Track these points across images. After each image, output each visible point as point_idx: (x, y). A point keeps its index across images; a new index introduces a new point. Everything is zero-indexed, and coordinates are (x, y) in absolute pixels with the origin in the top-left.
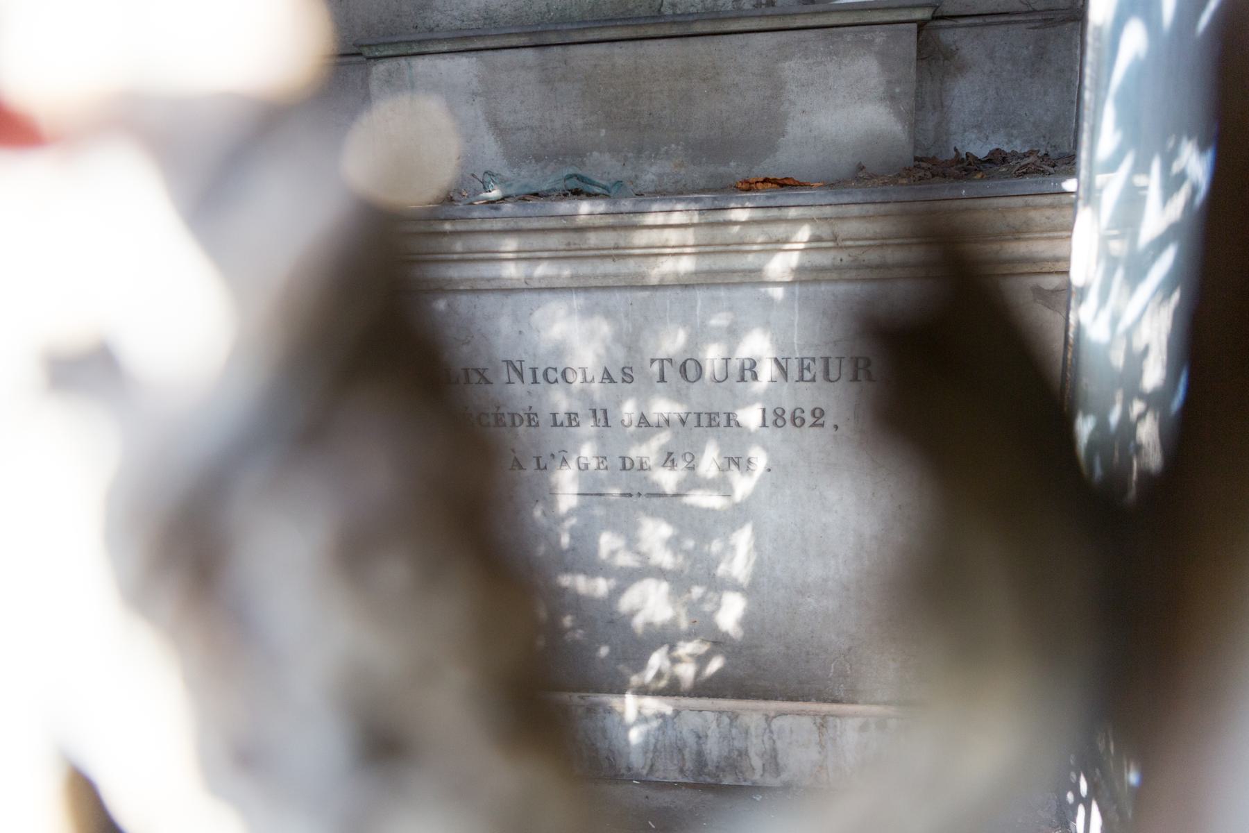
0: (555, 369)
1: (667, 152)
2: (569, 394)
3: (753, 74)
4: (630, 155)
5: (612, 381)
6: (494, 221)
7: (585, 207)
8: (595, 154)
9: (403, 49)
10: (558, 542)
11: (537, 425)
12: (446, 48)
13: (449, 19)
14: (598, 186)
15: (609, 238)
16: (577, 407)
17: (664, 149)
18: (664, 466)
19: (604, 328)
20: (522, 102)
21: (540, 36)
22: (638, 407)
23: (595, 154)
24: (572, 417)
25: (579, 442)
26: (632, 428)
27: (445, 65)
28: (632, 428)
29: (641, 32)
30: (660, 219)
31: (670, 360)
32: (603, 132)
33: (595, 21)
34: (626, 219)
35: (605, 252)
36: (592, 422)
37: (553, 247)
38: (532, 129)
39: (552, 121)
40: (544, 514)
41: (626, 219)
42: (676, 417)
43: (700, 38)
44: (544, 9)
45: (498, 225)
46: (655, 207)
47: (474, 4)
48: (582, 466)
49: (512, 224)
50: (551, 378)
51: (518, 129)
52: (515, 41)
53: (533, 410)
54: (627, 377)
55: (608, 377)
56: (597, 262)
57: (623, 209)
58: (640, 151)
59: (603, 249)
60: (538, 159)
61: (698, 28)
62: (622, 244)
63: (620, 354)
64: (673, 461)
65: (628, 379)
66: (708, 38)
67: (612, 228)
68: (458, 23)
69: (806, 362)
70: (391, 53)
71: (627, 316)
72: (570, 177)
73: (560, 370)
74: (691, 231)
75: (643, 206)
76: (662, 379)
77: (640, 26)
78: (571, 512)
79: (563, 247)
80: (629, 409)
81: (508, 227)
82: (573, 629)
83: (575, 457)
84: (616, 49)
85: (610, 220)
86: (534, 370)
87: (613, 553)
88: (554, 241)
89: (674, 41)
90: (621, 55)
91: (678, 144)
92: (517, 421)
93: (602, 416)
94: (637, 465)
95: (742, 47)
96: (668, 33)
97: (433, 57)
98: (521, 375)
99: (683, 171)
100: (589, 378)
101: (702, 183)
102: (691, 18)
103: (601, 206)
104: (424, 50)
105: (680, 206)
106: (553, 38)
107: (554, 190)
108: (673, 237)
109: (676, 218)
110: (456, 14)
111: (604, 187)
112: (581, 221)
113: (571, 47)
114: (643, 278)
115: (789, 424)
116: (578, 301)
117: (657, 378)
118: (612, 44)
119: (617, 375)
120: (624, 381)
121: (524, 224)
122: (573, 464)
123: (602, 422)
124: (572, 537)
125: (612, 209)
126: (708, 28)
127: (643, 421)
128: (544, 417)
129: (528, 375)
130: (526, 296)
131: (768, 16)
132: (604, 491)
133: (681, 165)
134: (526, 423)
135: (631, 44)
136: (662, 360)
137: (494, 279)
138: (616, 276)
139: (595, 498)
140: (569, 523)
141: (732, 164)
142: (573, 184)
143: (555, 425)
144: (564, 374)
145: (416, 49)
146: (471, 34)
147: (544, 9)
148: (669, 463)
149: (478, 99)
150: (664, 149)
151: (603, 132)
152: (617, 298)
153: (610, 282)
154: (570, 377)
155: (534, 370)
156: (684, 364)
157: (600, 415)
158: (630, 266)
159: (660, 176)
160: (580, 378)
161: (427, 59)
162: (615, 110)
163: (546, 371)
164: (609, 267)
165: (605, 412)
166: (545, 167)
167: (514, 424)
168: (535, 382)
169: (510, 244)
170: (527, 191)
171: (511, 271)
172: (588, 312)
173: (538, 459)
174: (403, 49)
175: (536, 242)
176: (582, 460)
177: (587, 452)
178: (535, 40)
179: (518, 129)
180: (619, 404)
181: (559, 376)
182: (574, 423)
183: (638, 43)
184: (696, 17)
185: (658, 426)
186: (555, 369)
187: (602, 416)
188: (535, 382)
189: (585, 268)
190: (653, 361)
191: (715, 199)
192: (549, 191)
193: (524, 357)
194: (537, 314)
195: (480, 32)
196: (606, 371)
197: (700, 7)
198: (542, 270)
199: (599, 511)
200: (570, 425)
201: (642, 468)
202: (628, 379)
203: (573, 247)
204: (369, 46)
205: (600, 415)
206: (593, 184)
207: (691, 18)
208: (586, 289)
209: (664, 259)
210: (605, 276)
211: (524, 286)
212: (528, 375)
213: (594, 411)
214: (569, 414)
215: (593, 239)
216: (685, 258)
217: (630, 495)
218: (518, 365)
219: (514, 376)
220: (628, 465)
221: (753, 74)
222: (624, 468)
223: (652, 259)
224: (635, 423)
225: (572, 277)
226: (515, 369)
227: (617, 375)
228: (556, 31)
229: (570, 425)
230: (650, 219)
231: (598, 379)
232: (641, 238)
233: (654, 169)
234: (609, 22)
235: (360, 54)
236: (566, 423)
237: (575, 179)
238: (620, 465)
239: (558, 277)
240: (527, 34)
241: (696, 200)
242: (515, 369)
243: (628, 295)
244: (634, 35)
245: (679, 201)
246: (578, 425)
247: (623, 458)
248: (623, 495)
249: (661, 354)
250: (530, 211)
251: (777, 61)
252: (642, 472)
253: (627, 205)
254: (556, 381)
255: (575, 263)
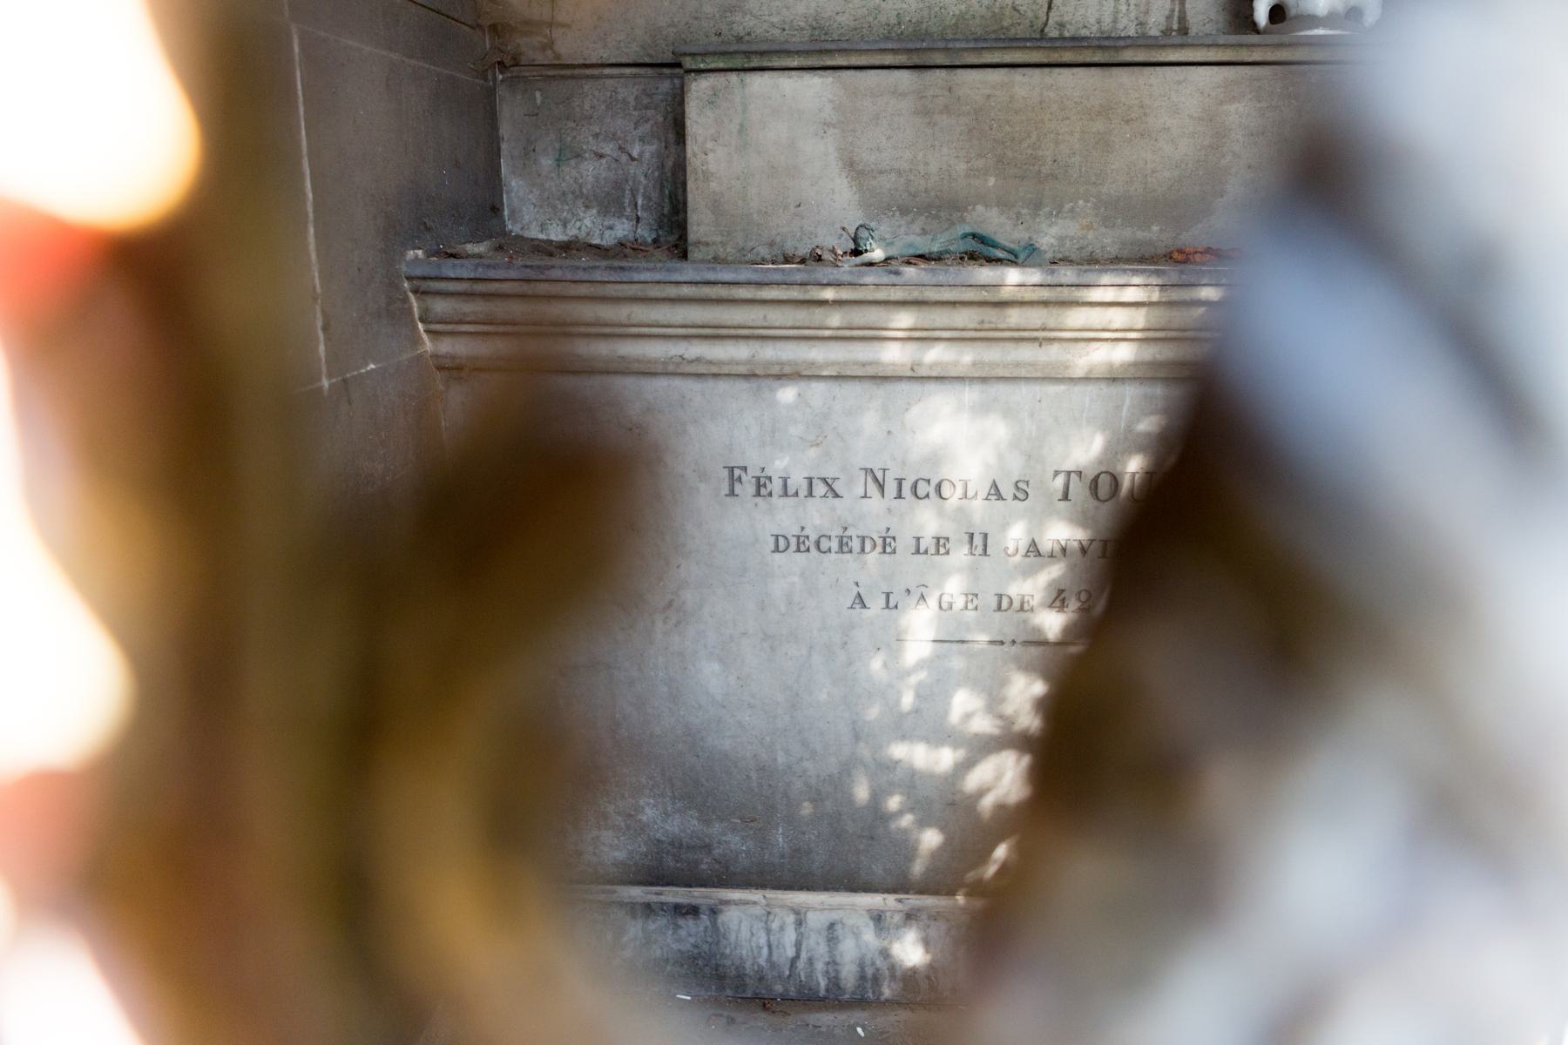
0: (929, 481)
1: (1072, 210)
2: (941, 513)
3: (1191, 117)
4: (1024, 211)
5: (1000, 497)
6: (893, 289)
7: (1013, 276)
8: (979, 208)
9: (739, 62)
10: (898, 702)
11: (894, 552)
12: (795, 64)
13: (765, 26)
14: (1004, 249)
15: (1035, 317)
16: (948, 529)
17: (1068, 206)
18: (1050, 606)
19: (999, 429)
20: (889, 138)
21: (920, 51)
22: (1029, 531)
23: (979, 208)
24: (941, 543)
25: (944, 575)
26: (1018, 558)
27: (789, 85)
28: (1018, 558)
29: (1055, 57)
30: (1109, 295)
31: (1080, 473)
32: (992, 181)
33: (997, 40)
34: (1065, 294)
35: (1026, 334)
36: (966, 549)
37: (961, 325)
38: (899, 173)
39: (926, 164)
40: (885, 665)
41: (1065, 294)
42: (1076, 544)
43: (1126, 69)
44: (893, 21)
45: (897, 294)
46: (1106, 279)
47: (801, 9)
48: (945, 606)
49: (916, 294)
50: (921, 492)
51: (881, 172)
52: (888, 59)
53: (891, 533)
54: (1021, 492)
55: (996, 492)
56: (1010, 346)
57: (1064, 280)
58: (1037, 206)
59: (606, 325)
60: (904, 211)
61: (1128, 56)
62: (1052, 324)
63: (1016, 466)
64: (1063, 601)
65: (1021, 496)
66: (1136, 69)
67: (1045, 303)
68: (777, 32)
69: (737, 472)
70: (721, 65)
71: (1032, 415)
72: (965, 236)
73: (934, 483)
74: (1143, 311)
75: (1089, 278)
76: (1066, 497)
77: (1055, 49)
78: (920, 665)
79: (972, 326)
80: (1017, 535)
81: (909, 298)
82: (900, 813)
83: (938, 594)
84: (1018, 76)
85: (1045, 294)
86: (900, 482)
87: (968, 716)
88: (963, 318)
89: (1093, 69)
90: (1026, 85)
91: (1087, 201)
92: (868, 547)
93: (980, 543)
94: (1016, 605)
95: (1179, 83)
96: (1088, 60)
97: (775, 74)
98: (881, 487)
99: (1090, 235)
100: (970, 494)
101: (1113, 250)
102: (1122, 43)
103: (1035, 276)
104: (766, 64)
105: (1137, 280)
106: (940, 59)
107: (947, 252)
108: (1118, 317)
109: (1131, 295)
110: (775, 20)
111: (1010, 252)
112: (1006, 294)
113: (959, 71)
114: (1067, 367)
115: (813, 549)
116: (971, 394)
117: (1060, 495)
118: (1012, 71)
119: (1007, 490)
120: (1016, 497)
121: (932, 294)
122: (932, 602)
123: (980, 550)
124: (918, 696)
125: (1050, 280)
126: (1141, 56)
127: (1034, 549)
128: (904, 543)
129: (891, 488)
130: (904, 387)
131: (1218, 46)
132: (969, 638)
133: (1089, 227)
134: (879, 549)
135: (1037, 71)
136: (1069, 473)
137: (871, 364)
138: (1032, 365)
139: (955, 647)
140: (913, 680)
141: (1155, 228)
142: (971, 245)
143: (918, 552)
144: (939, 487)
145: (755, 63)
146: (833, 46)
147: (893, 21)
148: (1058, 603)
149: (831, 131)
150: (1068, 206)
151: (992, 181)
152: (1023, 394)
153: (1023, 373)
154: (946, 491)
155: (900, 482)
156: (1095, 481)
157: (978, 540)
158: (1053, 353)
159: (1061, 239)
160: (959, 492)
161: (767, 75)
162: (1010, 154)
163: (916, 484)
164: (1026, 353)
165: (986, 536)
166: (913, 221)
167: (863, 550)
168: (899, 496)
169: (904, 319)
170: (911, 251)
171: (893, 355)
172: (982, 410)
173: (888, 595)
174: (739, 62)
175: (940, 317)
176: (946, 599)
177: (954, 588)
178: (916, 60)
179: (881, 172)
180: (1005, 526)
181: (932, 490)
182: (942, 550)
183: (1047, 70)
184: (1129, 42)
185: (1052, 556)
186: (929, 481)
187: (980, 543)
188: (899, 496)
189: (992, 354)
190: (1057, 473)
191: (1182, 272)
192: (941, 253)
193: (889, 465)
194: (915, 410)
195: (845, 46)
196: (995, 485)
197: (1094, 29)
198: (936, 355)
199: (957, 663)
200: (938, 552)
201: (1022, 609)
202: (1021, 496)
203: (986, 326)
204: (693, 55)
205: (978, 540)
206: (995, 245)
207: (1122, 43)
208: (984, 380)
209: (1098, 344)
210: (1018, 365)
211: (909, 374)
212: (891, 488)
213: (972, 536)
214: (938, 539)
215: (1014, 317)
216: (1124, 345)
217: (1002, 643)
218: (879, 475)
219: (873, 489)
220: (1005, 605)
221: (1191, 117)
222: (999, 608)
223: (1082, 344)
224: (1022, 551)
225: (974, 364)
226: (876, 479)
227: (1007, 490)
228: (946, 49)
229: (938, 552)
230: (1096, 295)
231: (983, 494)
232: (1077, 318)
233: (1054, 230)
234: (1014, 42)
235: (679, 65)
236: (932, 550)
237: (970, 239)
238: (994, 605)
239: (956, 364)
240: (909, 51)
241: (1157, 273)
242: (876, 479)
243: (1037, 389)
244: (1045, 60)
245: (1135, 272)
246: (947, 553)
247: (1000, 596)
248: (992, 642)
249: (1069, 465)
250: (941, 278)
251: (1221, 103)
252: (1022, 615)
253: (1067, 274)
254: (927, 496)
255: (979, 347)
